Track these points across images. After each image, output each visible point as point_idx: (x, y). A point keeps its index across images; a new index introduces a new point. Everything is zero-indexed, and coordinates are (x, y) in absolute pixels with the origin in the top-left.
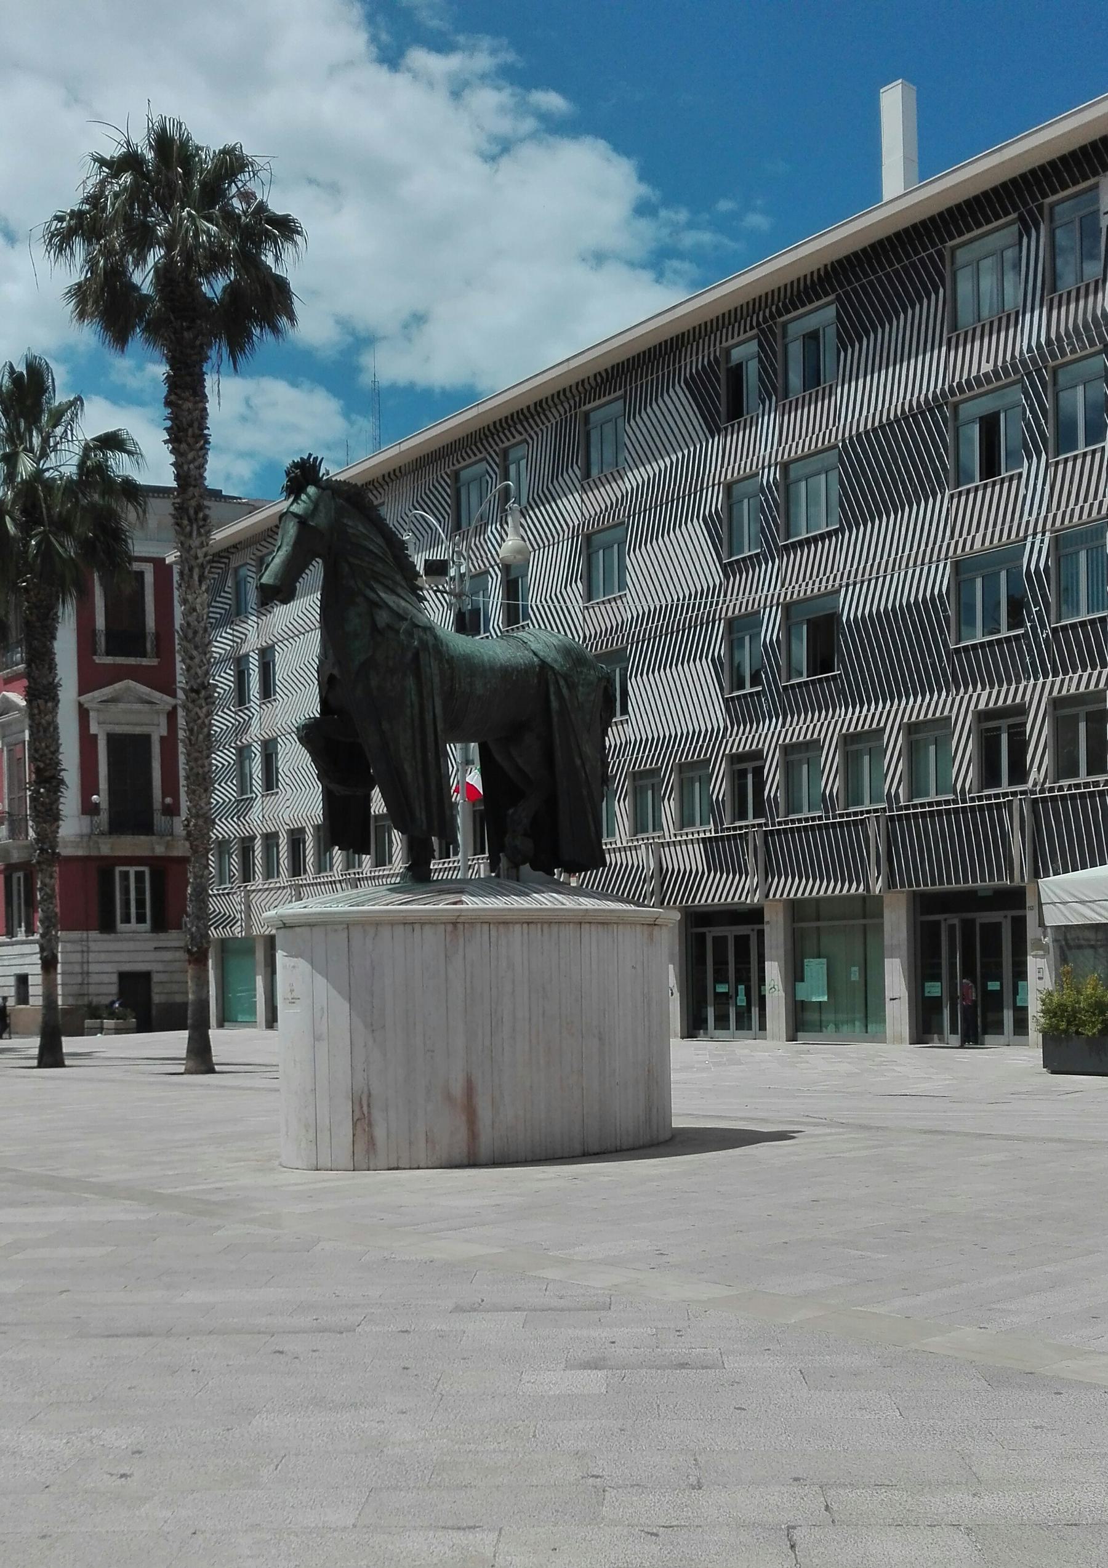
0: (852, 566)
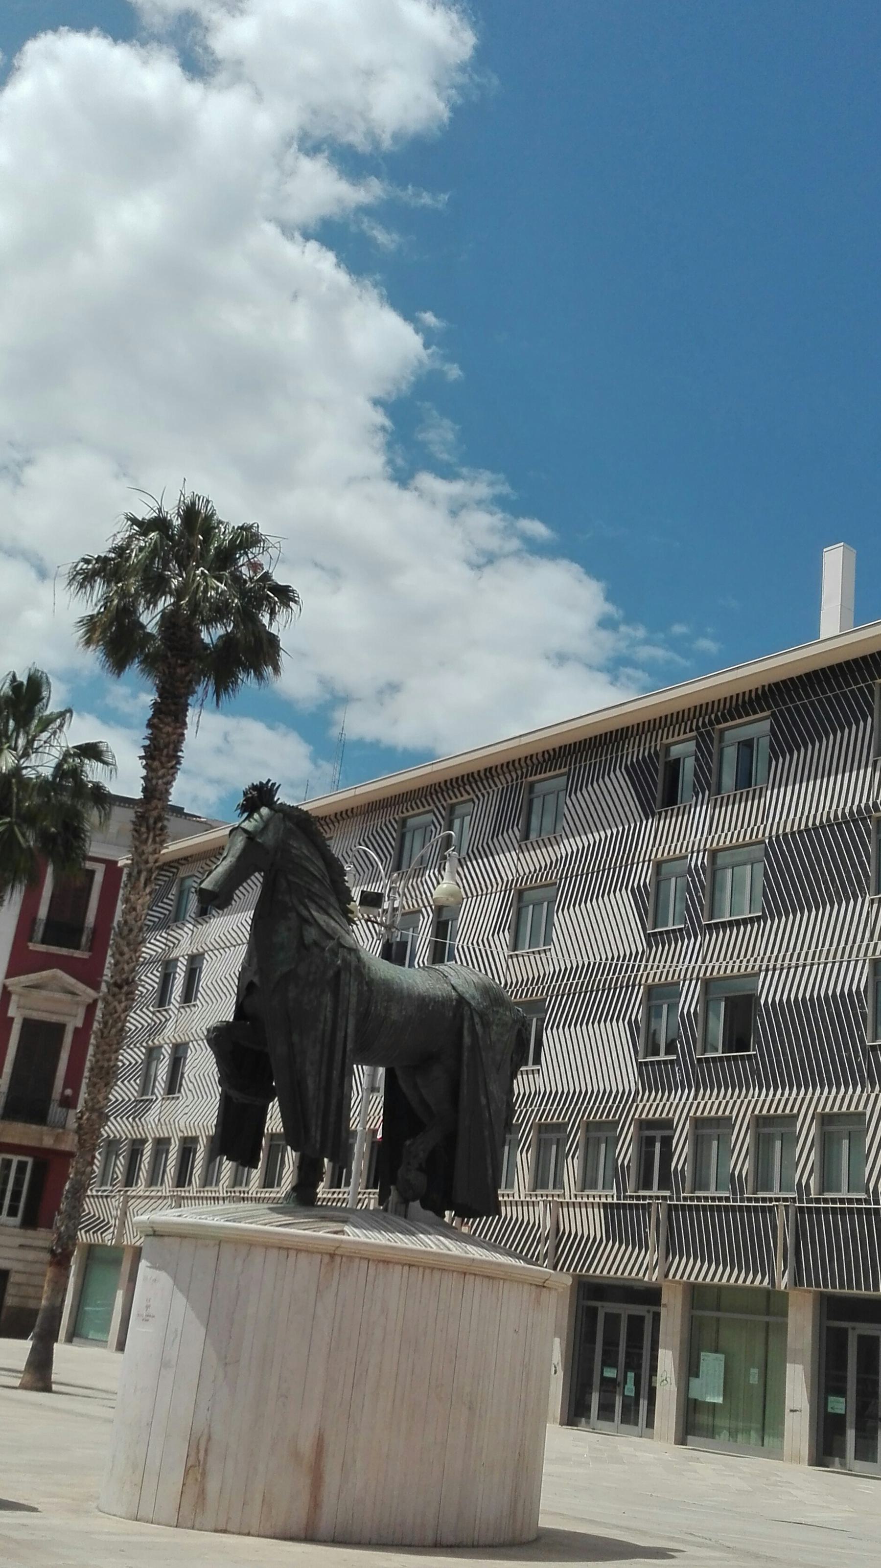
0: (772, 953)
